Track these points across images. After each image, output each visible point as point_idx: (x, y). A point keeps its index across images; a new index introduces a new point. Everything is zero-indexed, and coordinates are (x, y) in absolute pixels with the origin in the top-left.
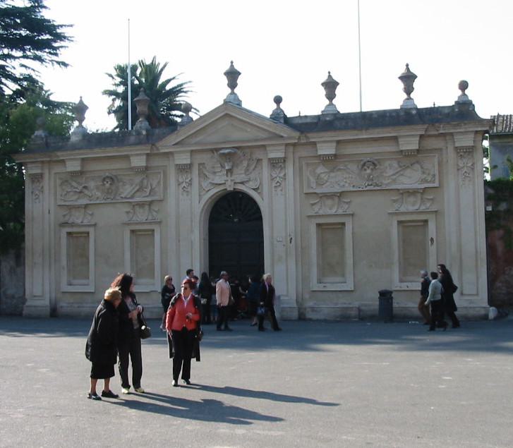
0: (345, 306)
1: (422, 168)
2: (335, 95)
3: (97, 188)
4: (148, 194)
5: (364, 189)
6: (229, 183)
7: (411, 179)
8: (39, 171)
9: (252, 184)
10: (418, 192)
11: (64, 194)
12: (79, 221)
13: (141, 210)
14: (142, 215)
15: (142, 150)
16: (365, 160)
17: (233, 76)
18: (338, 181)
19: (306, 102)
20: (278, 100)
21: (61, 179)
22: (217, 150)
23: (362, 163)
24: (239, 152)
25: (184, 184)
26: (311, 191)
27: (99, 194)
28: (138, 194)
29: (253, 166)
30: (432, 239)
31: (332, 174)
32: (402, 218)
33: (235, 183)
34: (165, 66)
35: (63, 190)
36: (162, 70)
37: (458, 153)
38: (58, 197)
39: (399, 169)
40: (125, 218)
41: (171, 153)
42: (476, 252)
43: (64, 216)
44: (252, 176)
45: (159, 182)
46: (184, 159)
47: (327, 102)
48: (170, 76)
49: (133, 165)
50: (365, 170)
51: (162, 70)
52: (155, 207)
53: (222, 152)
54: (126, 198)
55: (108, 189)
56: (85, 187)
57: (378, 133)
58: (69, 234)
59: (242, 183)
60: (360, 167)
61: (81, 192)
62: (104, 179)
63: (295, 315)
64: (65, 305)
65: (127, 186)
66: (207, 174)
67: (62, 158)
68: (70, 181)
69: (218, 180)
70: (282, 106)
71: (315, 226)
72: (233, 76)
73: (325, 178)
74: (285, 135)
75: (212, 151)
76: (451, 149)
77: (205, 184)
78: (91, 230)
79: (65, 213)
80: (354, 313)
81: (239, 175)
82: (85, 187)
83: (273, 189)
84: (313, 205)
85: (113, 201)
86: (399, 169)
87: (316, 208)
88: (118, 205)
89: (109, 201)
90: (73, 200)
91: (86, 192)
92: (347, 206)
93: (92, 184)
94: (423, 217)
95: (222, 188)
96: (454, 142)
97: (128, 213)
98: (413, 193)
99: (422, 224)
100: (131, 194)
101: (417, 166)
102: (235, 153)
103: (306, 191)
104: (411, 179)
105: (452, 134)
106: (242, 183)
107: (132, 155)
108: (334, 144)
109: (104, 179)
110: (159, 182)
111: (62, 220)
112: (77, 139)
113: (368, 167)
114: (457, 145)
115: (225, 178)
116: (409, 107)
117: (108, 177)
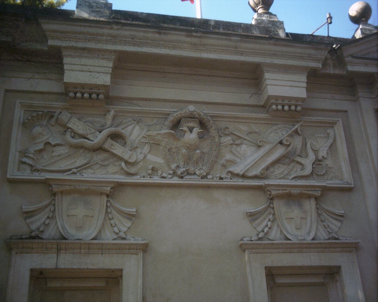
4: (308, 170)
10: (309, 197)
12: (88, 234)
13: (295, 212)
27: (156, 159)
28: (279, 170)
40: (247, 231)
43: (29, 214)
45: (332, 147)
52: (127, 202)
55: (191, 148)
56: (116, 137)
61: (99, 149)
62: (176, 125)
68: (65, 116)
71: (339, 265)
85: (205, 182)
88: (217, 194)
89: (187, 180)
91: (118, 149)
92: (128, 224)
93: (135, 133)
99: (101, 284)
107: (66, 48)
109: (176, 125)
110: (332, 147)
113: (191, 130)
117: (191, 117)
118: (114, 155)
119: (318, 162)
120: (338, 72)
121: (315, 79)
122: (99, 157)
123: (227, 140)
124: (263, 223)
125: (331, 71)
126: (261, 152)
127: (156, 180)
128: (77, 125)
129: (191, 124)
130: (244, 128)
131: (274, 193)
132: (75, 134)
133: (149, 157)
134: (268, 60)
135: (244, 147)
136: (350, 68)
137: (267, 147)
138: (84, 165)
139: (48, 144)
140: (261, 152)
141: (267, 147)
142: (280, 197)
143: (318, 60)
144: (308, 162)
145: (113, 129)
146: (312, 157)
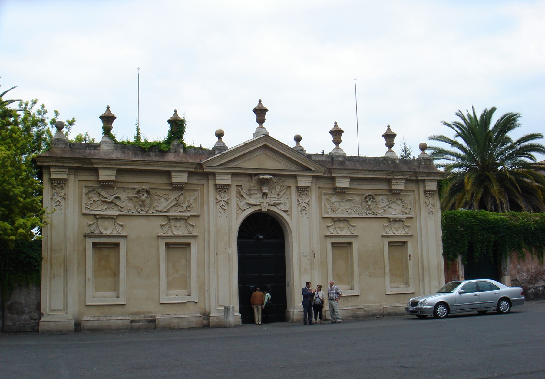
0: (353, 308)
1: (402, 203)
2: (341, 141)
3: (130, 199)
5: (367, 216)
6: (265, 204)
7: (395, 211)
8: (65, 177)
9: (282, 207)
11: (89, 203)
14: (179, 229)
15: (186, 167)
16: (367, 194)
17: (260, 112)
18: (344, 209)
19: (318, 144)
20: (220, 135)
21: (87, 187)
22: (256, 175)
23: (364, 196)
24: (275, 180)
25: (223, 203)
26: (328, 216)
27: (131, 205)
29: (283, 192)
30: (410, 256)
31: (342, 204)
32: (97, 240)
33: (269, 205)
34: (474, 110)
35: (89, 199)
36: (474, 113)
37: (217, 189)
38: (84, 206)
39: (388, 203)
41: (214, 174)
42: (438, 265)
44: (282, 200)
46: (222, 180)
47: (387, 149)
48: (519, 121)
49: (100, 179)
50: (367, 202)
51: (474, 113)
53: (261, 177)
54: (161, 212)
56: (117, 198)
57: (381, 175)
58: (94, 244)
59: (274, 205)
60: (363, 199)
61: (111, 202)
63: (72, 326)
64: (90, 318)
65: (162, 200)
66: (244, 195)
67: (95, 166)
69: (252, 201)
70: (301, 143)
72: (260, 112)
73: (338, 206)
74: (313, 169)
75: (250, 175)
76: (421, 190)
77: (242, 204)
78: (122, 242)
79: (90, 223)
80: (361, 313)
81: (272, 199)
82: (117, 198)
83: (300, 213)
84: (328, 227)
85: (147, 214)
86: (388, 203)
87: (331, 229)
90: (100, 209)
91: (118, 202)
94: (403, 239)
95: (257, 208)
96: (215, 180)
97: (162, 226)
98: (396, 221)
100: (168, 208)
101: (399, 202)
102: (271, 179)
103: (325, 215)
104: (395, 211)
105: (424, 181)
106: (274, 205)
108: (186, 174)
109: (138, 192)
111: (87, 230)
112: (108, 148)
113: (143, 195)
114: (427, 188)
115: (261, 200)
116: (394, 158)
117: (144, 189)
118: (116, 205)
119: (189, 206)
120: (201, 171)
121: (190, 174)
122: (111, 205)
123: (156, 197)
124: (166, 228)
125: (198, 171)
126: (168, 202)
127: (130, 213)
128: (103, 193)
129: (143, 193)
130: (163, 192)
131: (170, 218)
132: (103, 197)
133: (128, 204)
134: (173, 169)
135: (162, 200)
136: (205, 171)
137: (170, 201)
138: (108, 168)
139: (94, 200)
140: (168, 202)
141: (170, 201)
142: (172, 219)
143: (193, 168)
144: (185, 206)
145: (116, 195)
146: (187, 204)
